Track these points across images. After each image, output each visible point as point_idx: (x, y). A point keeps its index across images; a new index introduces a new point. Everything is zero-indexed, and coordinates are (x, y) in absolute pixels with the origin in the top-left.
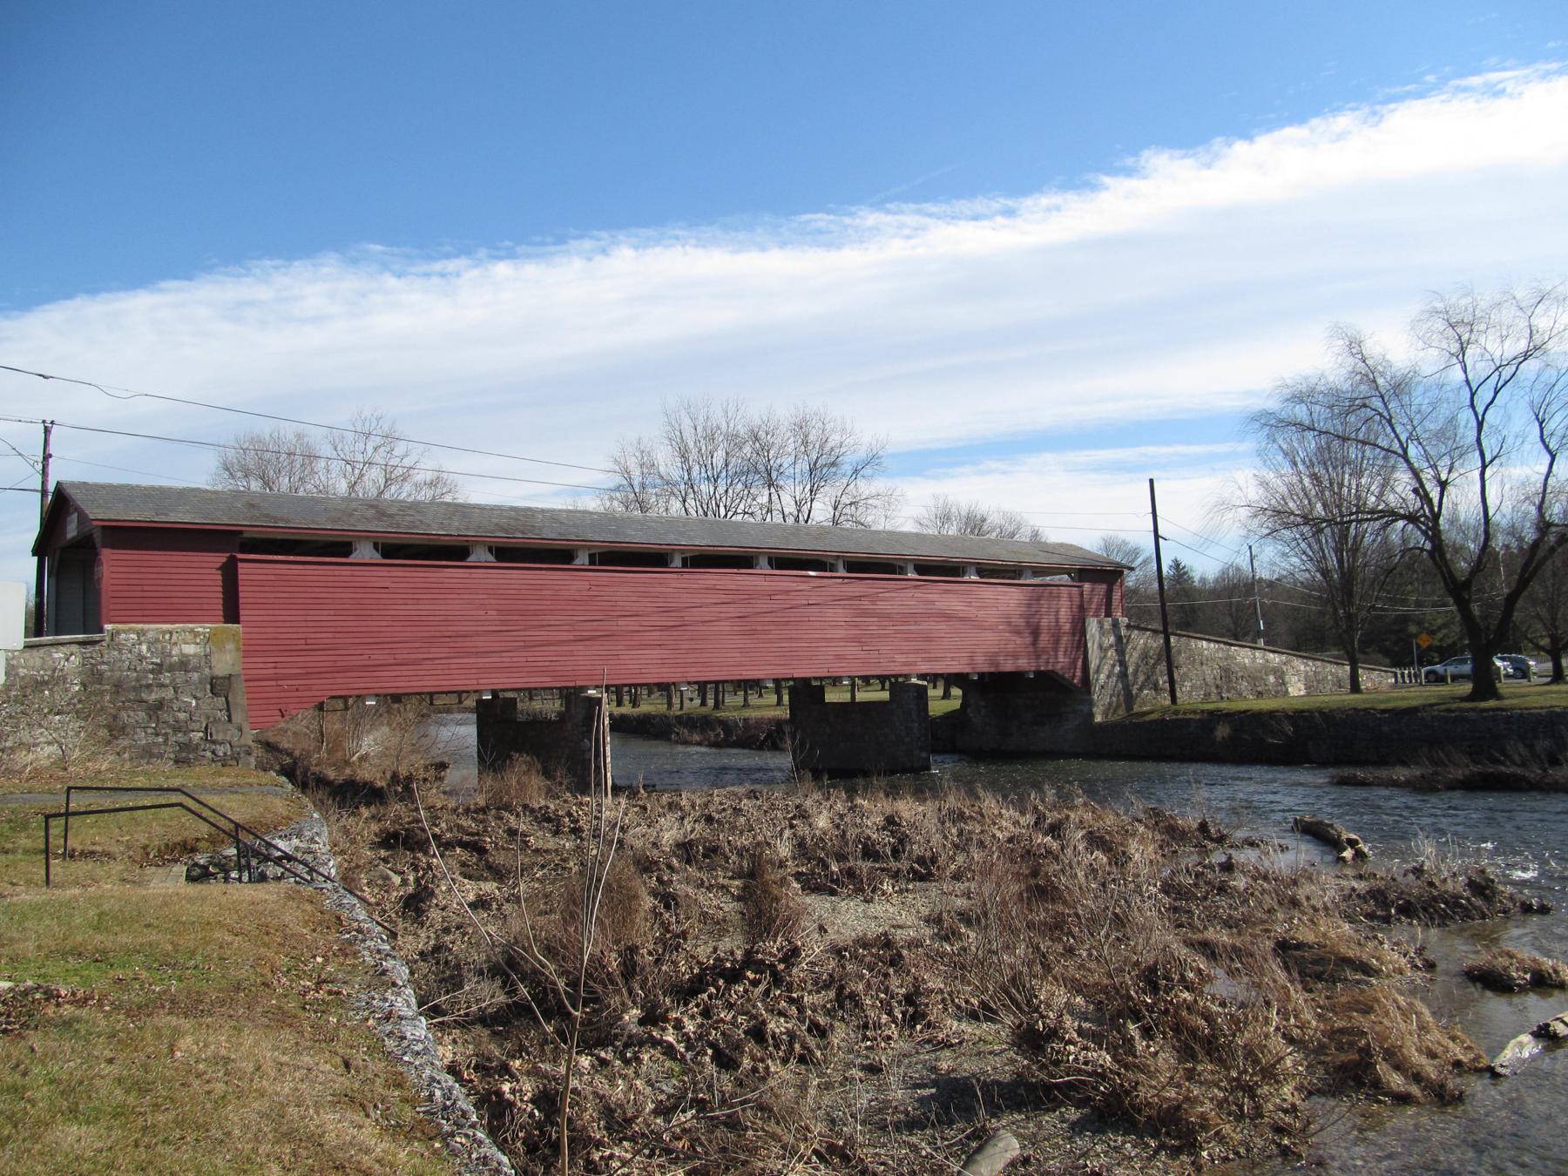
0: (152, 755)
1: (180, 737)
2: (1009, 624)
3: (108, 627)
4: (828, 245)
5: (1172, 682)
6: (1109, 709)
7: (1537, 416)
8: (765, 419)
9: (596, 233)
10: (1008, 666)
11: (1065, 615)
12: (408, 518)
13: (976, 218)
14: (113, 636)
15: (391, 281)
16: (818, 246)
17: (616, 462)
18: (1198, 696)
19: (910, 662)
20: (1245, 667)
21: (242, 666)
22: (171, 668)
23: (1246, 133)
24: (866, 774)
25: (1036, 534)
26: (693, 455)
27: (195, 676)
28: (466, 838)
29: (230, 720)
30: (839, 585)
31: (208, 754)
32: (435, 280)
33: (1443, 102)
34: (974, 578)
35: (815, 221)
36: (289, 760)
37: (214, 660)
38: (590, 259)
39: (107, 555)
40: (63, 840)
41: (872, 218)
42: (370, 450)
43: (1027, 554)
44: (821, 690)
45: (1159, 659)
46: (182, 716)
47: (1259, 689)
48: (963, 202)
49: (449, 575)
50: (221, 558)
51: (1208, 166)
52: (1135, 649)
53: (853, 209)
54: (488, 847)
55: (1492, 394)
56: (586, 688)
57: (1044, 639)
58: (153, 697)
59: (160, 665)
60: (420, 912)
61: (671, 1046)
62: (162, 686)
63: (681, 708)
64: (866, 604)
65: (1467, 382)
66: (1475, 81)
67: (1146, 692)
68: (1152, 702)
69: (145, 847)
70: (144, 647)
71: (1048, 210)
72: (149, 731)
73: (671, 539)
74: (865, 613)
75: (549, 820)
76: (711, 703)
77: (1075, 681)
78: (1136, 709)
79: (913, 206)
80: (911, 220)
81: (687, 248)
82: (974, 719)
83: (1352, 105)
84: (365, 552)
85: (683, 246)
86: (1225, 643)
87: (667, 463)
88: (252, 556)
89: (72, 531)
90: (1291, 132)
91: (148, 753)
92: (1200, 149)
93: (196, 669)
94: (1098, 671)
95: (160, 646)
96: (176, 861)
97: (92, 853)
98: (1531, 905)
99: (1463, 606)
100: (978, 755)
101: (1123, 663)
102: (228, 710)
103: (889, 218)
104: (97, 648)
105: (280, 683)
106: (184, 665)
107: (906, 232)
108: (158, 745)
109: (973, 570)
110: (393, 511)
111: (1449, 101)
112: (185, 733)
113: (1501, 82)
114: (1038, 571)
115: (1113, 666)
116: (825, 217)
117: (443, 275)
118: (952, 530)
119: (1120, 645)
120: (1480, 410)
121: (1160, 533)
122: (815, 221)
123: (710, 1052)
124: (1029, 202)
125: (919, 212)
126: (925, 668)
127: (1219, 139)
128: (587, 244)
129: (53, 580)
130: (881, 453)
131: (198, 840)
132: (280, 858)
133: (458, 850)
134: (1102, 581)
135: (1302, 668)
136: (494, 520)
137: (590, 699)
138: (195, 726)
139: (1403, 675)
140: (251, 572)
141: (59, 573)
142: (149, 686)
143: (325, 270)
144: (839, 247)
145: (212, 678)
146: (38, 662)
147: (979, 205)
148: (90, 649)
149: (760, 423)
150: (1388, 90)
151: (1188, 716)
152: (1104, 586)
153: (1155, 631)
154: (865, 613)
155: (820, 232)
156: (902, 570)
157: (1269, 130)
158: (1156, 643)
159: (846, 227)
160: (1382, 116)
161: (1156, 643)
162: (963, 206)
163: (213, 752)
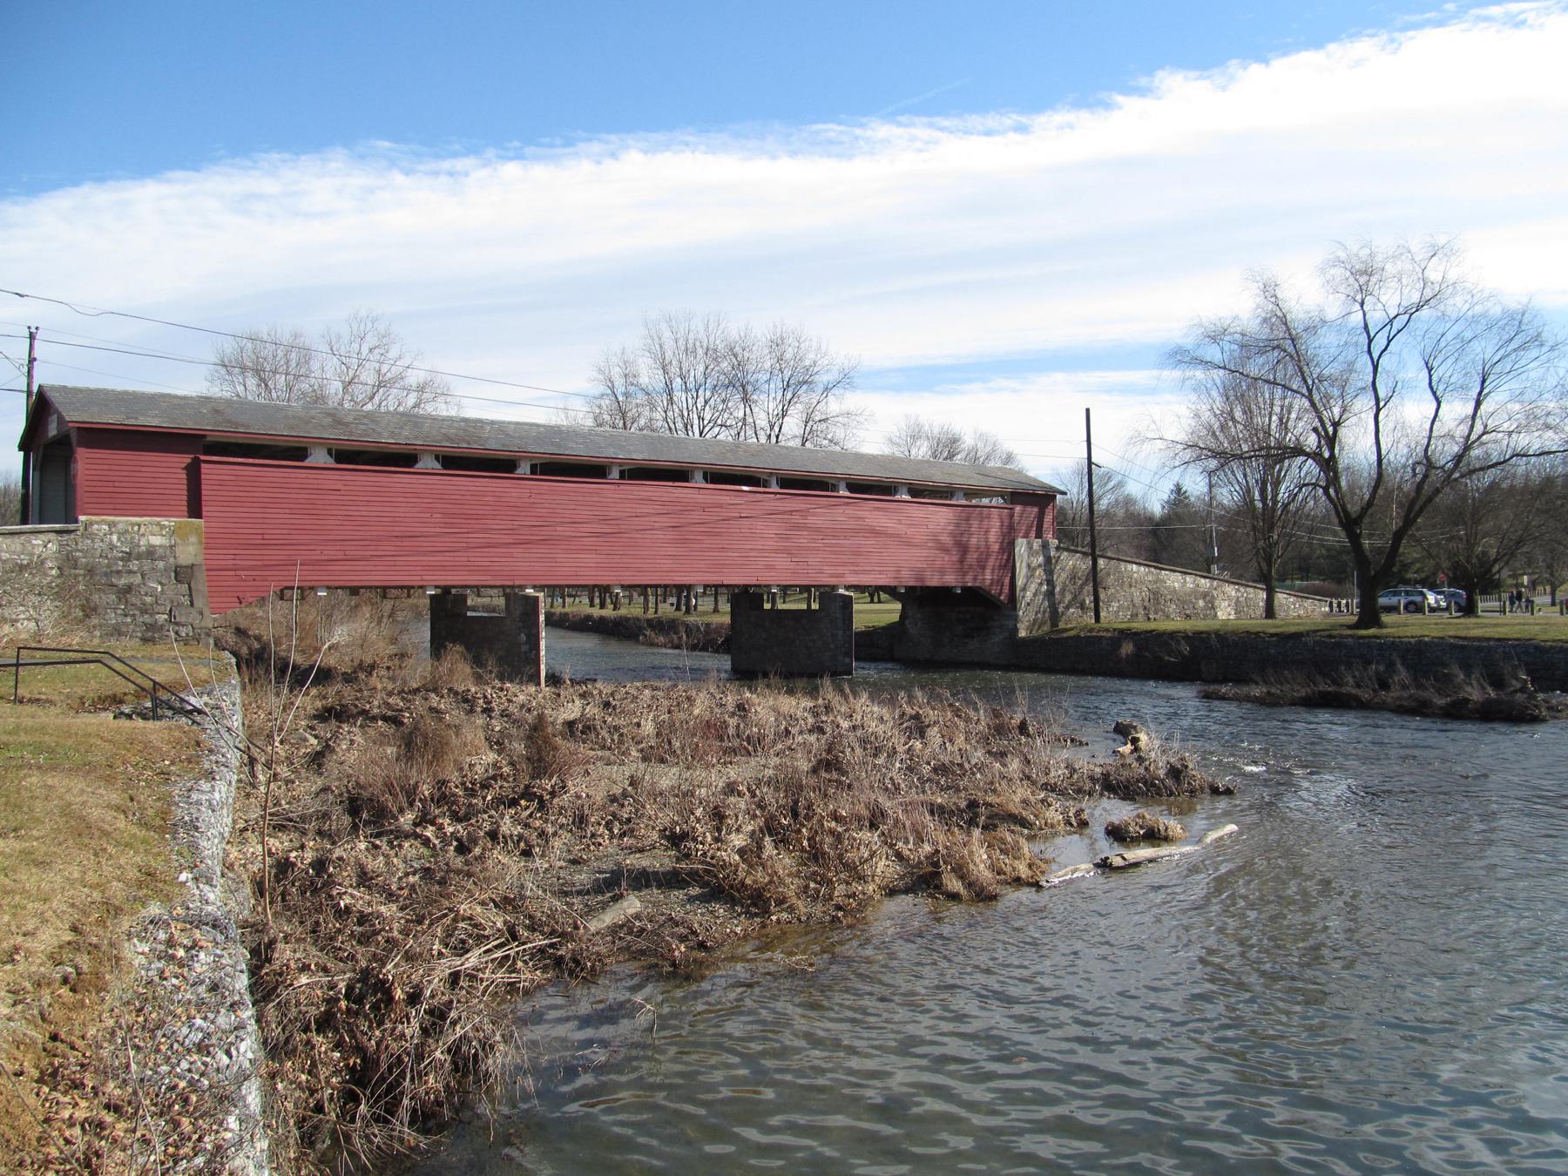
0: (120, 633)
1: (147, 618)
2: (938, 541)
3: (82, 518)
4: (839, 156)
5: (1097, 601)
6: (1034, 624)
7: (1427, 364)
8: (742, 334)
9: (604, 136)
10: (934, 581)
11: (994, 536)
12: (362, 427)
14: (87, 526)
15: (398, 178)
16: (829, 156)
17: (600, 371)
18: (1125, 615)
19: (842, 575)
21: (203, 557)
22: (139, 557)
23: (1261, 56)
24: (766, 675)
26: (674, 370)
27: (161, 564)
28: (390, 713)
29: (192, 604)
30: (772, 500)
32: (444, 179)
33: (1462, 31)
34: (906, 497)
35: (827, 131)
36: (256, 645)
37: (178, 550)
38: (599, 163)
41: (883, 131)
42: (365, 350)
45: (1087, 580)
46: (148, 599)
47: (1188, 612)
48: (974, 116)
49: (397, 481)
50: (186, 459)
52: (1063, 569)
53: (864, 120)
54: (406, 721)
55: (1385, 342)
56: (523, 587)
57: (972, 557)
58: (123, 582)
59: (129, 554)
60: (320, 766)
61: (428, 840)
62: (130, 572)
63: (656, 612)
64: (796, 518)
65: (1366, 327)
66: (1495, 10)
68: (1076, 620)
69: (82, 698)
70: (115, 537)
71: (1061, 128)
72: (119, 612)
73: (610, 452)
74: (797, 527)
75: (466, 701)
76: (652, 611)
78: (1061, 625)
79: (924, 120)
80: (923, 133)
81: (697, 153)
82: (911, 631)
83: (1370, 31)
84: (319, 457)
85: (693, 152)
86: (1156, 568)
87: (649, 376)
89: (53, 430)
91: (117, 632)
93: (162, 558)
94: (1024, 589)
95: (128, 537)
96: (105, 710)
97: (38, 700)
98: (1218, 788)
99: (1355, 538)
101: (1050, 582)
102: (191, 595)
103: (900, 131)
104: (72, 536)
105: (239, 573)
106: (151, 553)
107: (918, 145)
108: (127, 625)
109: (905, 489)
110: (350, 419)
111: (1469, 30)
112: (151, 615)
113: (1519, 14)
114: (971, 493)
115: (1041, 584)
116: (836, 127)
117: (451, 174)
118: (922, 451)
120: (1375, 356)
121: (1094, 460)
122: (827, 131)
123: (455, 843)
124: (1042, 119)
125: (931, 125)
127: (1234, 62)
128: (596, 147)
129: (37, 474)
130: (852, 373)
131: (125, 694)
132: (191, 712)
133: (380, 723)
136: (443, 431)
137: (527, 597)
138: (161, 609)
139: (1339, 605)
140: (214, 472)
141: (42, 467)
142: (118, 572)
143: (333, 165)
144: (851, 158)
145: (176, 567)
147: (992, 121)
148: (66, 537)
149: (737, 338)
150: (1406, 18)
151: (1101, 634)
152: (1036, 510)
153: (1084, 554)
154: (797, 527)
155: (831, 142)
156: (834, 488)
157: (1285, 54)
158: (1084, 565)
159: (857, 138)
160: (1400, 44)
161: (1084, 565)
162: (975, 121)
163: (177, 633)
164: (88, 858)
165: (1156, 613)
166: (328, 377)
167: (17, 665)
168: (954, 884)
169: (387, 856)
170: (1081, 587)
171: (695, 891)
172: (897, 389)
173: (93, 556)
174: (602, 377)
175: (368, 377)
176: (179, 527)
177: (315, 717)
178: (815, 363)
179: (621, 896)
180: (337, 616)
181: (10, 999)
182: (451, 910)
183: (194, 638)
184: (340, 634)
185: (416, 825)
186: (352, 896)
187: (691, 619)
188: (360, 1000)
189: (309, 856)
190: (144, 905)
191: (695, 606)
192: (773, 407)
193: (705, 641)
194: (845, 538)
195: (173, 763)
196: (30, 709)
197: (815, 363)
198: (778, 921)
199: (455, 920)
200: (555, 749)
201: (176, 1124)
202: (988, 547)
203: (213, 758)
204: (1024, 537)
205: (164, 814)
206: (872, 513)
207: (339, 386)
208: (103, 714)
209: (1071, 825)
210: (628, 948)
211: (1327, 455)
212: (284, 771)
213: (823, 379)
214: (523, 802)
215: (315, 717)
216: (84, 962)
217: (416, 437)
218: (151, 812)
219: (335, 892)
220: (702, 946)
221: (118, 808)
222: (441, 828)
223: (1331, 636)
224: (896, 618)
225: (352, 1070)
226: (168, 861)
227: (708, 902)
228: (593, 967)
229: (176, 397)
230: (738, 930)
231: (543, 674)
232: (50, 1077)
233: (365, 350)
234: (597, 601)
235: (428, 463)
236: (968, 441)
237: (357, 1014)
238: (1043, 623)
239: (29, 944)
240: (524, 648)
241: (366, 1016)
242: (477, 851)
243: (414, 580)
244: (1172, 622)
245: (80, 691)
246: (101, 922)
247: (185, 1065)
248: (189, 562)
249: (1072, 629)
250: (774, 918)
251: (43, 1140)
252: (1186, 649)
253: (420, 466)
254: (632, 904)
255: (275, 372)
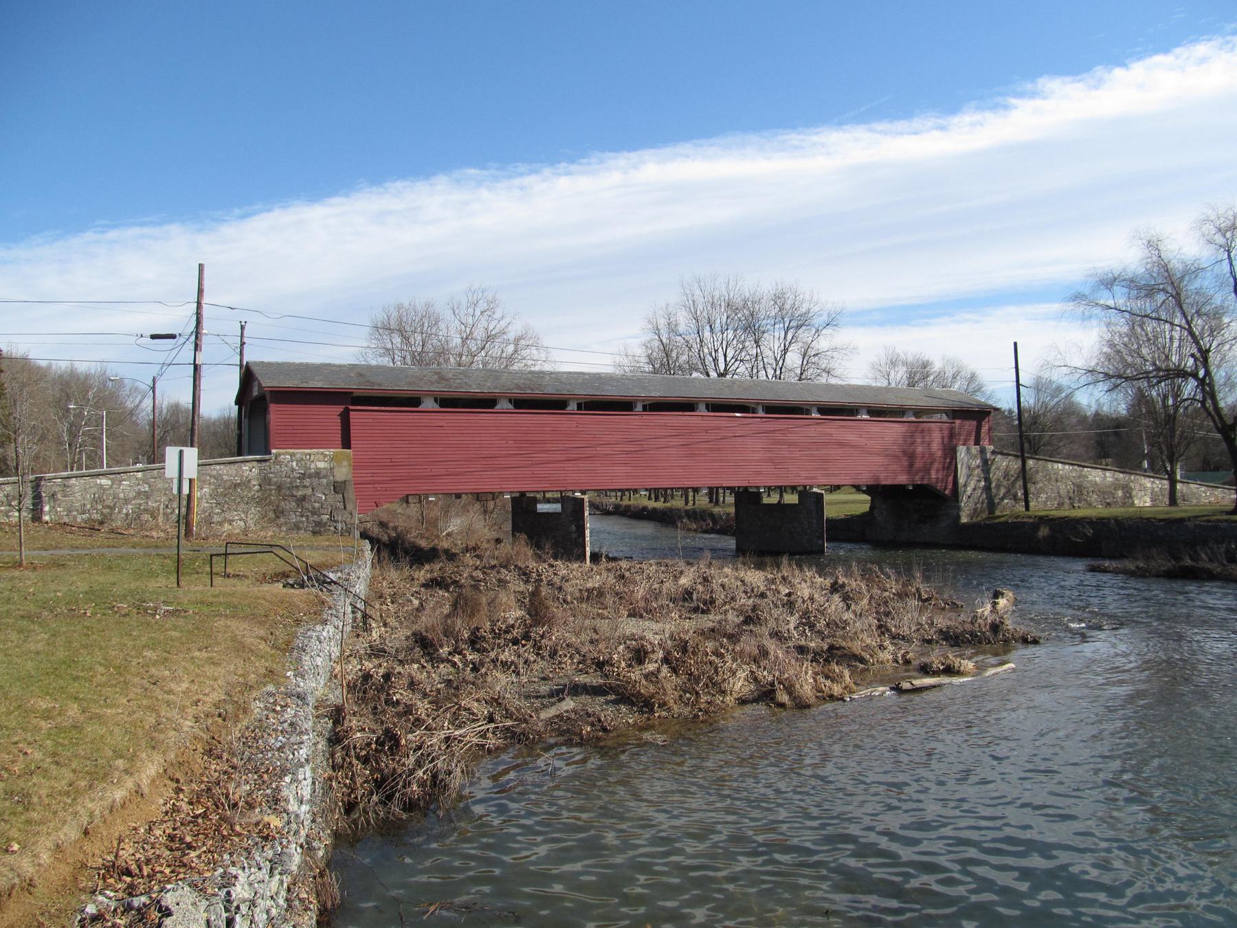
0: (299, 528)
1: (316, 518)
3: (274, 451)
5: (1026, 494)
11: (936, 446)
13: (916, 133)
14: (277, 456)
15: (484, 193)
20: (1096, 483)
22: (310, 476)
23: (1120, 61)
25: (973, 377)
27: (325, 481)
29: (345, 508)
30: (759, 423)
31: (332, 528)
34: (865, 417)
39: (273, 408)
40: (208, 566)
42: (478, 313)
43: (912, 399)
44: (535, 501)
45: (1018, 477)
46: (317, 505)
47: (1108, 501)
49: (483, 418)
50: (340, 409)
51: (1096, 88)
52: (998, 469)
57: (918, 464)
59: (304, 474)
61: (455, 663)
64: (779, 436)
67: (1006, 501)
68: (1009, 509)
69: (264, 574)
70: (294, 463)
75: (525, 574)
76: (691, 503)
77: (947, 492)
78: (998, 513)
83: (1206, 37)
84: (429, 404)
86: (1079, 466)
87: (684, 322)
88: (359, 408)
89: (255, 393)
90: (1159, 58)
92: (1085, 75)
93: (325, 477)
94: (965, 486)
98: (1027, 639)
100: (881, 544)
101: (987, 480)
106: (318, 474)
108: (303, 522)
109: (865, 411)
110: (450, 375)
112: (319, 515)
114: (918, 412)
115: (979, 481)
117: (521, 188)
119: (986, 466)
124: (955, 120)
125: (870, 130)
126: (823, 481)
127: (1099, 68)
134: (973, 419)
135: (1149, 485)
137: (576, 499)
138: (325, 511)
140: (359, 417)
142: (297, 487)
146: (234, 473)
148: (264, 464)
151: (1025, 520)
153: (1016, 456)
156: (808, 412)
157: (1139, 59)
158: (1016, 465)
161: (1016, 465)
164: (240, 663)
165: (1080, 501)
166: (451, 333)
167: (226, 554)
168: (783, 697)
169: (428, 673)
170: (1014, 483)
171: (612, 697)
172: (880, 324)
173: (281, 477)
174: (650, 326)
175: (479, 333)
176: (336, 455)
177: (424, 585)
178: (809, 310)
179: (564, 699)
180: (453, 511)
181: (194, 720)
182: (456, 704)
183: (346, 531)
184: (455, 525)
185: (450, 653)
186: (401, 694)
187: (716, 510)
188: (382, 744)
189: (382, 671)
190: (265, 685)
191: (724, 502)
192: (777, 346)
193: (717, 526)
194: (817, 449)
195: (305, 615)
196: (232, 581)
197: (809, 310)
198: (659, 717)
199: (459, 709)
200: (547, 608)
201: (261, 777)
202: (931, 455)
203: (330, 612)
204: (964, 445)
205: (288, 643)
206: (837, 429)
207: (459, 341)
208: (276, 584)
209: (897, 662)
210: (558, 729)
211: (1201, 373)
212: (392, 621)
213: (818, 321)
214: (523, 642)
215: (424, 585)
216: (230, 708)
217: (495, 388)
218: (281, 641)
219: (391, 692)
220: (605, 730)
221: (262, 638)
222: (464, 656)
223: (1209, 521)
224: (866, 508)
225: (376, 781)
226: (284, 666)
227: (618, 704)
228: (534, 738)
229: (334, 365)
230: (631, 721)
231: (588, 554)
232: (209, 752)
233: (478, 313)
234: (653, 496)
235: (504, 405)
236: (937, 366)
237: (381, 751)
238: (982, 511)
239: (205, 698)
240: (574, 536)
241: (385, 753)
242: (483, 670)
243: (495, 488)
244: (1095, 509)
245: (264, 570)
246: (242, 692)
247: (270, 755)
248: (343, 479)
249: (1003, 516)
250: (656, 715)
251: (202, 775)
252: (1090, 532)
253: (498, 407)
254: (569, 704)
255: (414, 332)
